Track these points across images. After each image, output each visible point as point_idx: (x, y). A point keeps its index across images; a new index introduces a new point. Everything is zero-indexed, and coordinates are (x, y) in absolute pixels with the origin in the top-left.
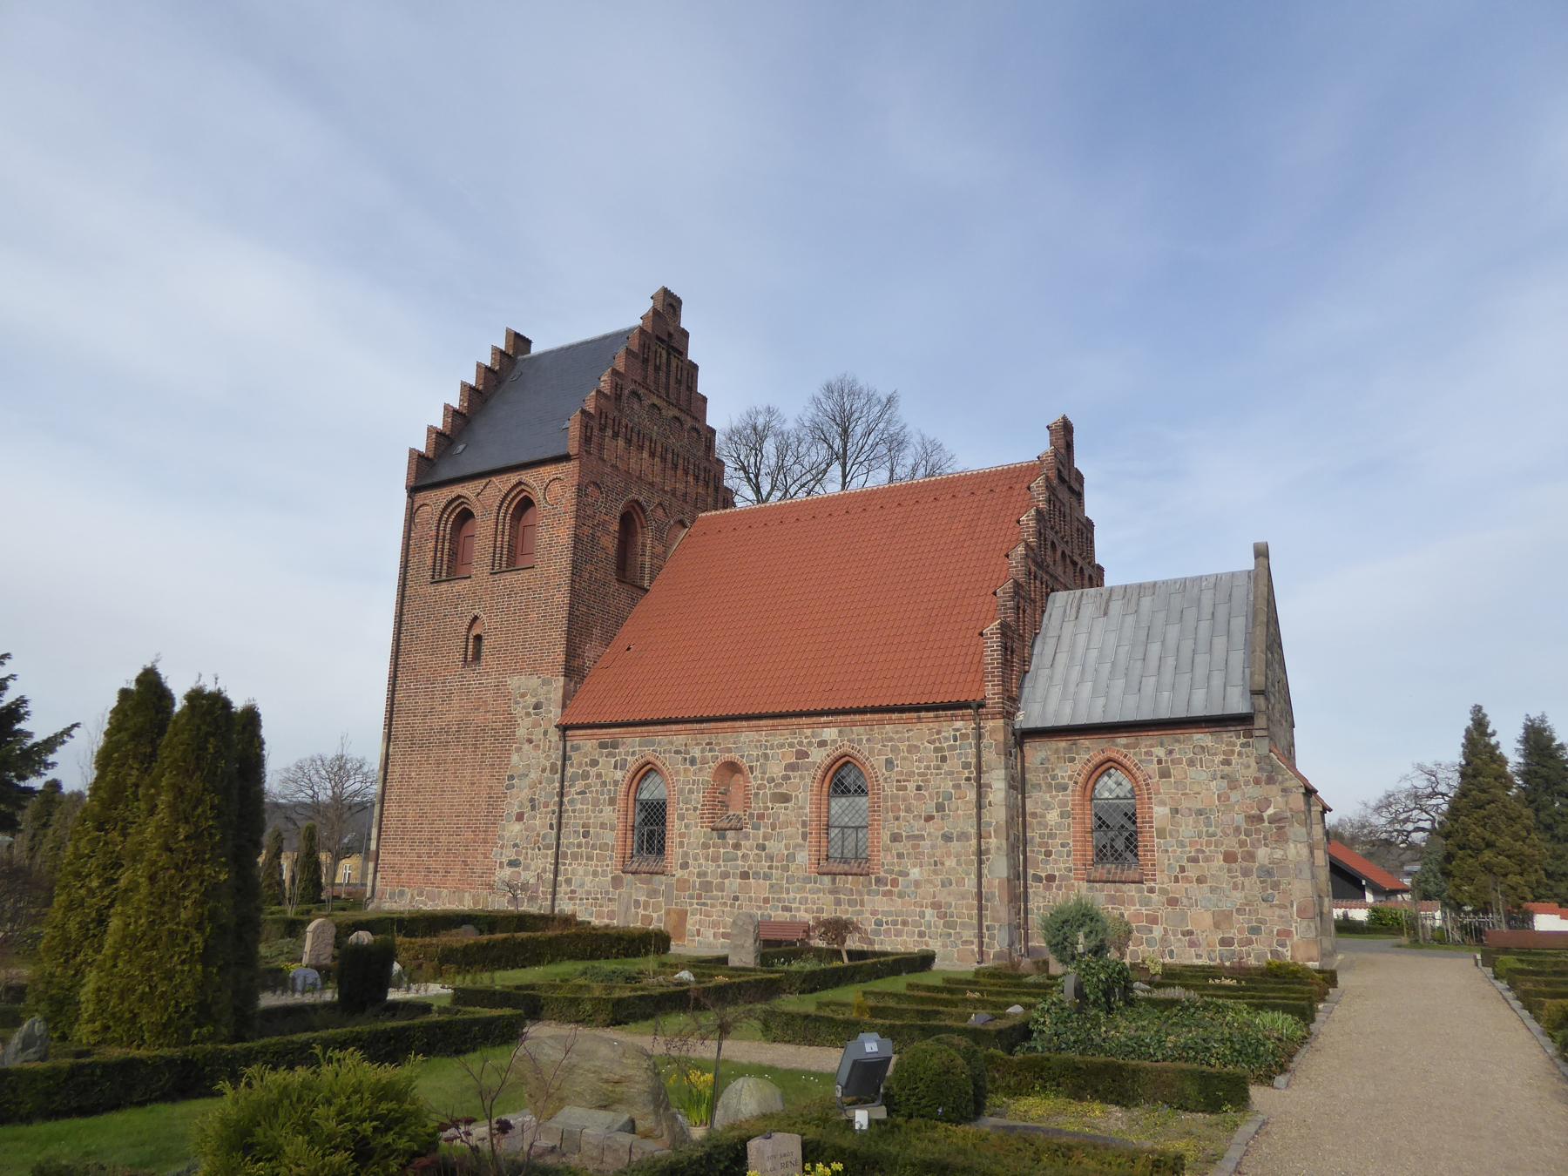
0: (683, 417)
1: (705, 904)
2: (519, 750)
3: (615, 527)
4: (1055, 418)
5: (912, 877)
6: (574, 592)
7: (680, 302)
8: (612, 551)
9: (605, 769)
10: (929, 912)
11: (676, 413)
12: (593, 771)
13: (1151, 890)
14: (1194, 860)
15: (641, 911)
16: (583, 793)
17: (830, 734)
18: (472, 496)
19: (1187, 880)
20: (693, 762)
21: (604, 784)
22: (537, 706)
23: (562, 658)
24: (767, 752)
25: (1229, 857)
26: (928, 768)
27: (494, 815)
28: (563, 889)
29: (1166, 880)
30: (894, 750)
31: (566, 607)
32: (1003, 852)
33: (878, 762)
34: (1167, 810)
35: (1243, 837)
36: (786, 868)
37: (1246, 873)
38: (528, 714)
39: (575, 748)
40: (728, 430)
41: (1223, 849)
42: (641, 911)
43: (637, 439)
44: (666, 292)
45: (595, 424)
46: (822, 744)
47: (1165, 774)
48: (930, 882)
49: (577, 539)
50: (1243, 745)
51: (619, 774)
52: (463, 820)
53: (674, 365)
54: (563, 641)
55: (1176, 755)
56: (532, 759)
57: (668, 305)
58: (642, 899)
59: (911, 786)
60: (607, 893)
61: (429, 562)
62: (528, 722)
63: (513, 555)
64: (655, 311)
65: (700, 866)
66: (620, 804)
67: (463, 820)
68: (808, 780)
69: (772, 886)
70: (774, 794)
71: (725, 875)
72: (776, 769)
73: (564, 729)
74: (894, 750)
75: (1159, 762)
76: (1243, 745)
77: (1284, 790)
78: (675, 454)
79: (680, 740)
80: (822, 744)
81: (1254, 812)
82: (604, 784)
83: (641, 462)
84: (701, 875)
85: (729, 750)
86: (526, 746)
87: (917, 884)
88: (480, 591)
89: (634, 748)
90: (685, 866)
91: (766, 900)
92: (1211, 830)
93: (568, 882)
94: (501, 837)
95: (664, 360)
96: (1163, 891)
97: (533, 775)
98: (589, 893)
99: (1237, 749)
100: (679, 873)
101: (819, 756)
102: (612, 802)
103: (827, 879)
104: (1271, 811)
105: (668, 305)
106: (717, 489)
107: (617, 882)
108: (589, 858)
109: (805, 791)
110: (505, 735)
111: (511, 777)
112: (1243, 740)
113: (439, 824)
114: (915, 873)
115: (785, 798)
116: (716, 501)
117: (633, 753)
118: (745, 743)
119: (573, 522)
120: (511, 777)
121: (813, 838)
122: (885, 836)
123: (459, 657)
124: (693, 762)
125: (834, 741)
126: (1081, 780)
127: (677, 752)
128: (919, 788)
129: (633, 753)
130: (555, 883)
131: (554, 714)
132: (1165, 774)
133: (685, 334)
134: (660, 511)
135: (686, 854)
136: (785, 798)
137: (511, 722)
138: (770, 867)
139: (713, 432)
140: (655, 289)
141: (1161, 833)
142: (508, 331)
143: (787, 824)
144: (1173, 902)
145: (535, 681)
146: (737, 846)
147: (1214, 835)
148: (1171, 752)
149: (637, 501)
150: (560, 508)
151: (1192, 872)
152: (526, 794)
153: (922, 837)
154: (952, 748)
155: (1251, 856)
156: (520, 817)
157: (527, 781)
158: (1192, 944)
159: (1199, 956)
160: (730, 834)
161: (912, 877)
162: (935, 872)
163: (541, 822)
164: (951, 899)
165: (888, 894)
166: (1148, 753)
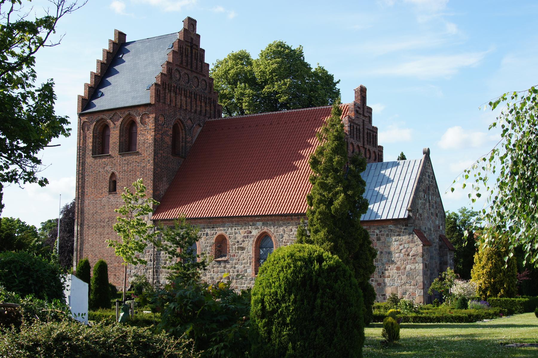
0: (198, 76)
3: (170, 132)
4: (357, 86)
6: (155, 164)
7: (195, 21)
8: (170, 143)
11: (195, 75)
23: (151, 192)
24: (236, 235)
29: (377, 277)
40: (215, 62)
44: (189, 18)
45: (161, 89)
47: (379, 239)
49: (155, 140)
50: (405, 229)
53: (194, 52)
55: (382, 233)
57: (191, 23)
64: (185, 30)
75: (377, 235)
76: (405, 229)
78: (196, 95)
88: (115, 162)
95: (189, 51)
96: (376, 281)
99: (403, 230)
106: (215, 106)
109: (250, 246)
112: (404, 227)
115: (243, 249)
118: (228, 232)
119: (153, 133)
121: (253, 264)
123: (107, 190)
132: (379, 239)
134: (189, 121)
136: (243, 249)
139: (208, 65)
140: (185, 17)
142: (116, 30)
146: (225, 267)
148: (381, 231)
149: (180, 119)
155: (405, 268)
166: (373, 232)
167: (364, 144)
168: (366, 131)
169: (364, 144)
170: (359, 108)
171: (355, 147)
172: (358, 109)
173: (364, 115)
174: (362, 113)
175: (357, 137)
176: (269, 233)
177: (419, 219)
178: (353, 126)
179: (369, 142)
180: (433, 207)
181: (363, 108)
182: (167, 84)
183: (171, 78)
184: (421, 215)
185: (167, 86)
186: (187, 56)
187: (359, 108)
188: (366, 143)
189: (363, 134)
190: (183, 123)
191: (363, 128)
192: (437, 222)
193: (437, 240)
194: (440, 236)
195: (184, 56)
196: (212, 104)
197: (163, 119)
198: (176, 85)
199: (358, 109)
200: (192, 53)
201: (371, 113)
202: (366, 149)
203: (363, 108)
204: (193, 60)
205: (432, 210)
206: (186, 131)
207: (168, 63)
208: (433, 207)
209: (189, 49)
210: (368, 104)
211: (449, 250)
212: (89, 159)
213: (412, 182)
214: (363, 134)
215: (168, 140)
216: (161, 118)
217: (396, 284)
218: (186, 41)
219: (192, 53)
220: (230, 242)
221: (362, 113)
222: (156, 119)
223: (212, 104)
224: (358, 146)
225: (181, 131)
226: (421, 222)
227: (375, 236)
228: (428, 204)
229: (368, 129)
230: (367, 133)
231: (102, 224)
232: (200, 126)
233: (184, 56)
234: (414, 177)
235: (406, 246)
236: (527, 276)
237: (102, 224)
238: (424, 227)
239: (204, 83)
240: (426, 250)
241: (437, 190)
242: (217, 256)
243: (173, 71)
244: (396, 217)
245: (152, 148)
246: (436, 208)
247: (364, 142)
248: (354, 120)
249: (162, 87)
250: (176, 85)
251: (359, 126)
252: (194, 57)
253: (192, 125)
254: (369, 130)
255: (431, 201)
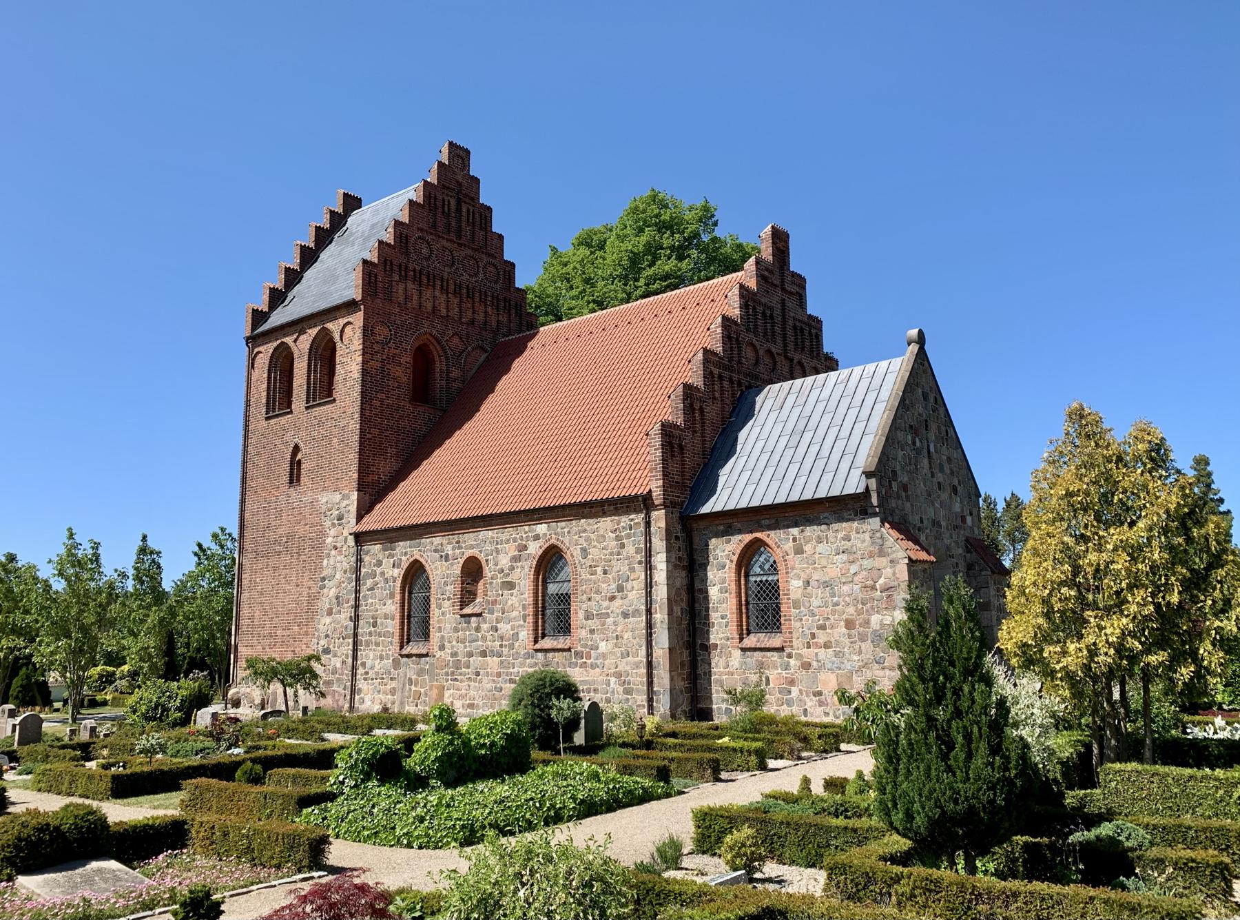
0: (477, 255)
1: (456, 680)
2: (328, 556)
5: (601, 650)
9: (388, 566)
10: (613, 680)
12: (379, 570)
13: (789, 656)
14: (823, 627)
15: (413, 688)
16: (371, 589)
17: (542, 529)
18: (291, 344)
19: (817, 646)
20: (447, 558)
21: (386, 581)
22: (340, 518)
25: (849, 624)
26: (611, 554)
27: (311, 611)
28: (360, 671)
29: (800, 646)
30: (588, 539)
31: (358, 432)
32: (665, 626)
33: (576, 551)
34: (801, 583)
35: (860, 606)
36: (511, 647)
37: (863, 638)
38: (333, 524)
39: (367, 553)
41: (844, 617)
42: (413, 688)
43: (424, 278)
46: (537, 538)
47: (799, 551)
48: (614, 654)
51: (396, 571)
52: (292, 617)
53: (464, 209)
54: (356, 461)
56: (338, 563)
57: (459, 154)
58: (414, 677)
59: (599, 570)
60: (390, 673)
61: (264, 401)
62: (333, 532)
63: (323, 389)
65: (452, 647)
66: (398, 597)
67: (292, 617)
68: (527, 570)
69: (502, 662)
70: (503, 583)
71: (470, 655)
72: (504, 561)
73: (359, 538)
74: (588, 539)
75: (794, 540)
77: (892, 561)
79: (437, 540)
80: (537, 538)
81: (869, 583)
82: (386, 581)
83: (432, 298)
84: (454, 654)
85: (472, 547)
86: (333, 552)
87: (604, 656)
88: (302, 421)
89: (406, 551)
90: (442, 648)
91: (499, 675)
92: (835, 600)
93: (363, 664)
94: (317, 630)
95: (453, 207)
96: (799, 656)
97: (338, 576)
98: (377, 673)
100: (438, 654)
101: (535, 549)
102: (392, 596)
103: (539, 654)
104: (881, 581)
105: (459, 154)
107: (396, 664)
108: (377, 644)
109: (524, 577)
110: (318, 545)
111: (323, 579)
113: (276, 621)
114: (603, 647)
115: (510, 586)
116: (521, 324)
117: (406, 554)
119: (360, 358)
120: (323, 579)
121: (530, 619)
122: (581, 615)
124: (447, 558)
125: (545, 535)
126: (735, 559)
127: (436, 551)
128: (605, 572)
129: (406, 554)
130: (354, 668)
131: (351, 525)
133: (477, 181)
134: (456, 340)
135: (443, 637)
137: (322, 534)
138: (501, 646)
141: (797, 605)
143: (513, 608)
144: (806, 666)
145: (338, 497)
146: (478, 629)
147: (837, 604)
150: (353, 348)
151: (822, 637)
152: (332, 593)
153: (607, 615)
154: (629, 536)
155: (867, 623)
156: (330, 613)
157: (335, 582)
158: (821, 704)
159: (827, 714)
160: (473, 619)
161: (601, 650)
162: (616, 645)
163: (345, 616)
164: (628, 668)
165: (583, 665)
167: (785, 350)
168: (791, 323)
169: (785, 350)
170: (770, 272)
171: (761, 352)
172: (766, 273)
173: (783, 289)
174: (777, 282)
175: (765, 333)
176: (562, 546)
177: (899, 497)
178: (754, 308)
179: (799, 347)
180: (942, 470)
181: (782, 275)
182: (395, 262)
183: (407, 254)
184: (905, 487)
185: (395, 268)
186: (449, 215)
187: (770, 272)
188: (791, 347)
189: (784, 329)
190: (439, 342)
191: (784, 316)
192: (957, 507)
193: (960, 551)
194: (967, 540)
195: (439, 214)
196: (513, 311)
197: (386, 331)
198: (418, 268)
199: (766, 273)
200: (459, 210)
201: (804, 288)
202: (791, 360)
203: (782, 275)
204: (464, 225)
205: (940, 477)
206: (447, 358)
207: (688, 389)
208: (942, 470)
209: (453, 202)
210: (795, 266)
211: (993, 572)
212: (259, 423)
213: (880, 408)
214: (784, 329)
215: (402, 374)
216: (381, 332)
217: (848, 666)
218: (444, 187)
219: (459, 210)
220: (488, 572)
221: (777, 282)
222: (367, 331)
223: (513, 311)
224: (769, 351)
225: (437, 358)
226: (908, 505)
227: (791, 544)
228: (925, 463)
229: (795, 319)
230: (795, 327)
231: (278, 548)
232: (486, 351)
233: (439, 214)
234: (885, 394)
235: (867, 563)
236: (953, 864)
237: (278, 548)
238: (917, 518)
239: (492, 269)
240: (920, 574)
241: (951, 432)
242: (463, 605)
243: (412, 240)
244: (835, 492)
245: (358, 388)
246: (952, 473)
247: (785, 346)
248: (755, 294)
249: (382, 268)
250: (418, 268)
251: (772, 309)
252: (464, 219)
253: (461, 346)
254: (800, 321)
255: (935, 456)
